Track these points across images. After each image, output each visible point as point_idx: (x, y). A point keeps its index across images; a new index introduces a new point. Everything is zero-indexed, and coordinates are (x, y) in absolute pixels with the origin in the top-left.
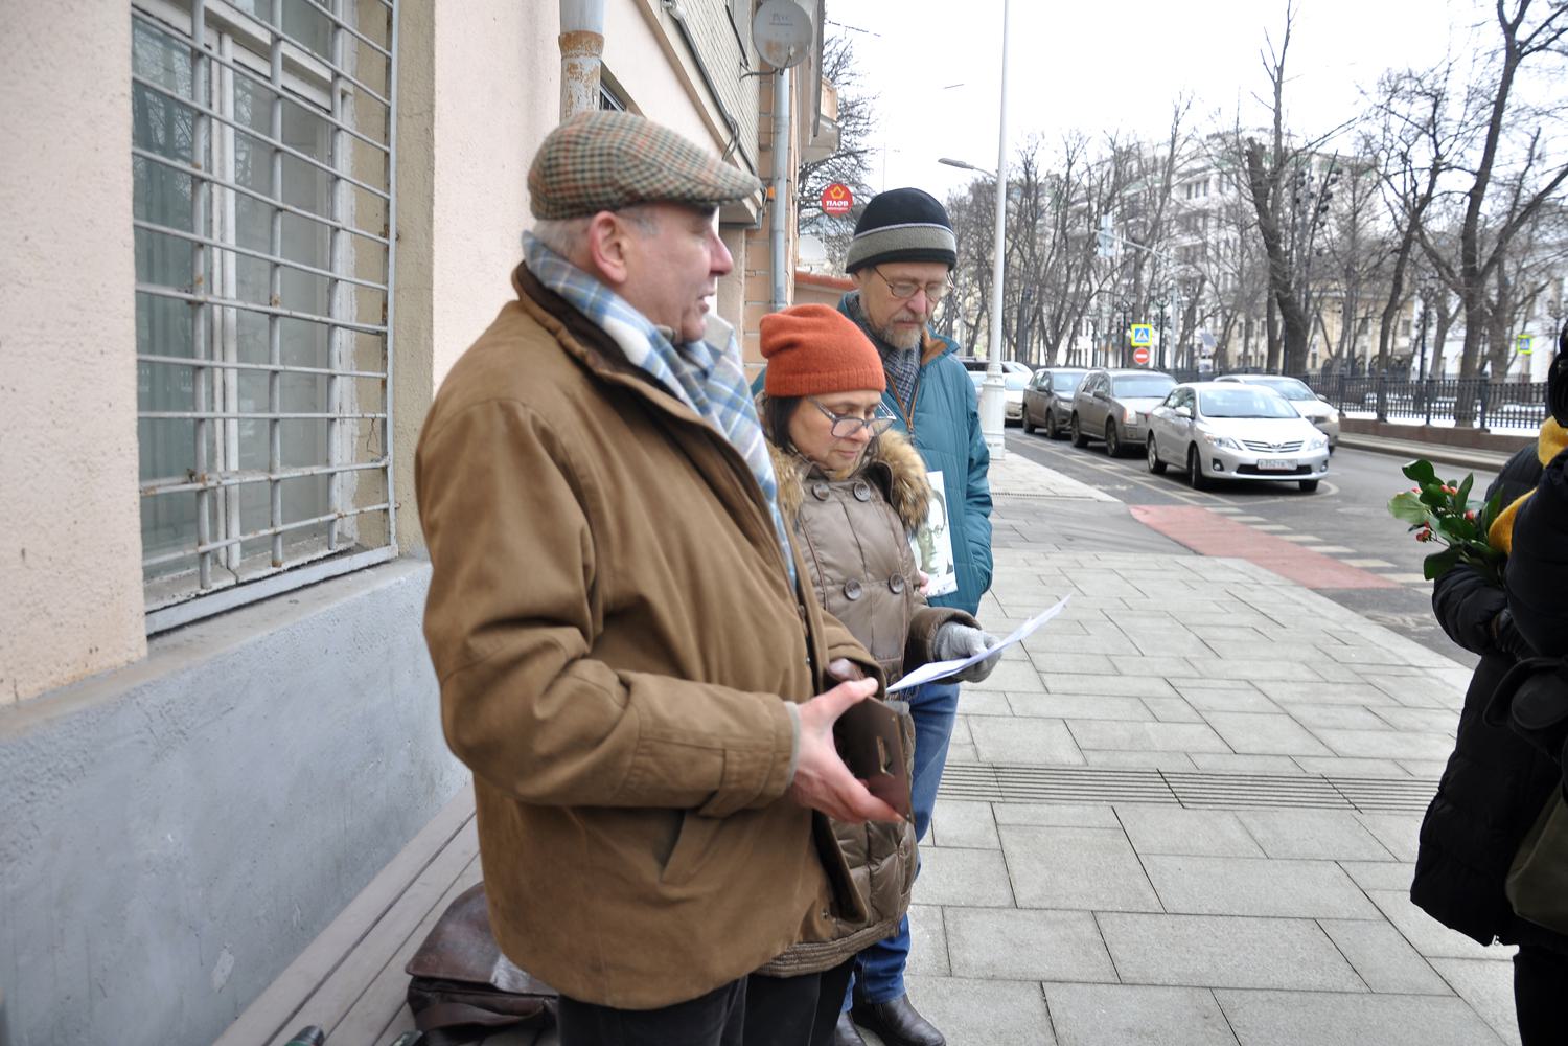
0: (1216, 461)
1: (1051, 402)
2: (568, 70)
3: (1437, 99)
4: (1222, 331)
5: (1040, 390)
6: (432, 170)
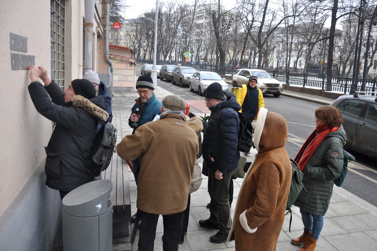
3: (253, 5)
4: (206, 53)
5: (164, 70)
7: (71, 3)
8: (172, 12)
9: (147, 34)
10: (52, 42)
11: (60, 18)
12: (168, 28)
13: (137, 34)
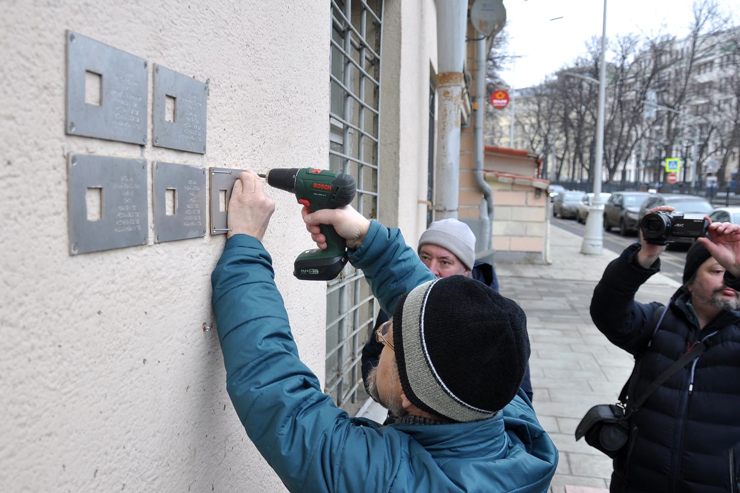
1: (623, 213)
2: (444, 95)
5: (616, 205)
6: (398, 176)
8: (630, 59)
9: (566, 120)
10: (333, 129)
11: (365, 53)
12: (620, 101)
13: (539, 122)
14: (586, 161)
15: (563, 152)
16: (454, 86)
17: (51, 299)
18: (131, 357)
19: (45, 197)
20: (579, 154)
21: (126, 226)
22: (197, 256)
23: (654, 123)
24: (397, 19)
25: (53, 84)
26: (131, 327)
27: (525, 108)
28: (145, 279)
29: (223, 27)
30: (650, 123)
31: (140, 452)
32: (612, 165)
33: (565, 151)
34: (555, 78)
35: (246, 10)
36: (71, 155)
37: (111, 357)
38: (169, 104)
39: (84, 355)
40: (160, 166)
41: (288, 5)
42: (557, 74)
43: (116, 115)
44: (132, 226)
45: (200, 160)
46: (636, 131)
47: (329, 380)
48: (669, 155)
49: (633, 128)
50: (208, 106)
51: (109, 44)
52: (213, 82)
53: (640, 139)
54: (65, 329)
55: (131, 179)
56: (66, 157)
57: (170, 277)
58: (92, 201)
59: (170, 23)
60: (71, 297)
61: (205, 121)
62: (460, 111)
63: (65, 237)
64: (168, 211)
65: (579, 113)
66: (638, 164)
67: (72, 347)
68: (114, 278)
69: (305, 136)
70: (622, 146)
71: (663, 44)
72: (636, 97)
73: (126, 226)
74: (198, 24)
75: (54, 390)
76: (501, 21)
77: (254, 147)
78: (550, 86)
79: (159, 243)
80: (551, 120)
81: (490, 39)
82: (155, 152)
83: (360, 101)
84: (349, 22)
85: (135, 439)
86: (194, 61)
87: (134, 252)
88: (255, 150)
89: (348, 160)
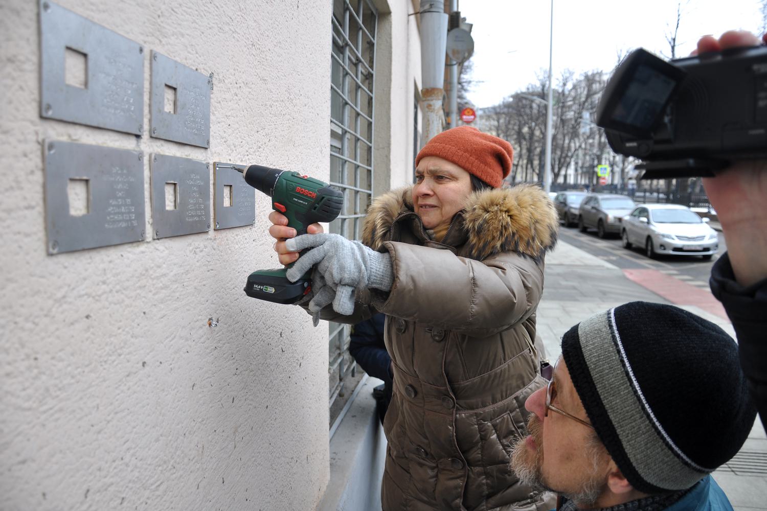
0: (662, 246)
1: (566, 209)
2: (427, 107)
5: (561, 203)
6: (389, 176)
7: (391, 27)
8: (569, 86)
10: (333, 134)
14: (536, 167)
15: (517, 159)
16: (436, 100)
17: (22, 306)
18: (128, 361)
19: (12, 188)
20: (530, 161)
21: (119, 221)
22: (201, 251)
23: (588, 137)
24: (388, 40)
25: (22, 58)
26: (127, 329)
27: (487, 123)
28: (143, 277)
29: (228, 23)
30: (585, 137)
31: (141, 460)
32: (556, 170)
33: (519, 159)
34: (511, 100)
35: (252, 11)
36: (47, 141)
37: (103, 364)
38: (169, 94)
39: (69, 365)
40: (157, 160)
41: (293, 12)
42: (513, 97)
43: (105, 100)
44: (126, 221)
45: (204, 154)
46: (575, 143)
47: (332, 359)
48: (600, 163)
49: (572, 141)
50: (212, 100)
51: (96, 20)
52: (217, 77)
53: (578, 150)
54: (43, 339)
55: (125, 171)
56: (42, 144)
57: (172, 274)
58: (76, 194)
59: (170, 10)
60: (51, 302)
61: (209, 115)
62: (441, 121)
63: (41, 234)
64: (168, 205)
65: (530, 128)
66: (576, 170)
67: (53, 358)
68: (105, 278)
69: (309, 136)
70: (564, 155)
71: (594, 75)
72: (575, 117)
73: (119, 221)
74: (201, 16)
75: (29, 409)
76: (470, 51)
77: (260, 145)
78: (507, 106)
79: (158, 239)
80: (508, 133)
81: (461, 65)
82: (153, 144)
83: (356, 109)
84: (347, 38)
85: (135, 448)
86: (197, 53)
87: (129, 249)
88: (260, 147)
89: (346, 161)
